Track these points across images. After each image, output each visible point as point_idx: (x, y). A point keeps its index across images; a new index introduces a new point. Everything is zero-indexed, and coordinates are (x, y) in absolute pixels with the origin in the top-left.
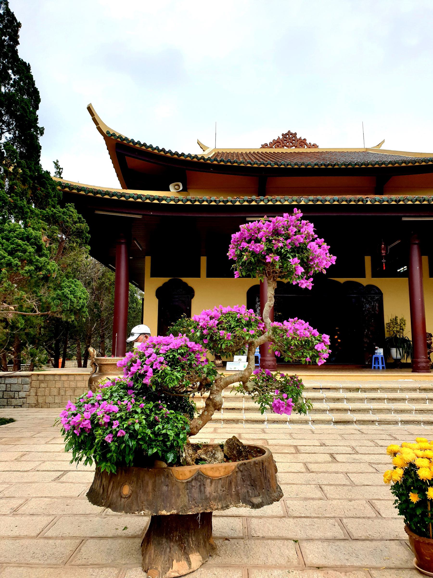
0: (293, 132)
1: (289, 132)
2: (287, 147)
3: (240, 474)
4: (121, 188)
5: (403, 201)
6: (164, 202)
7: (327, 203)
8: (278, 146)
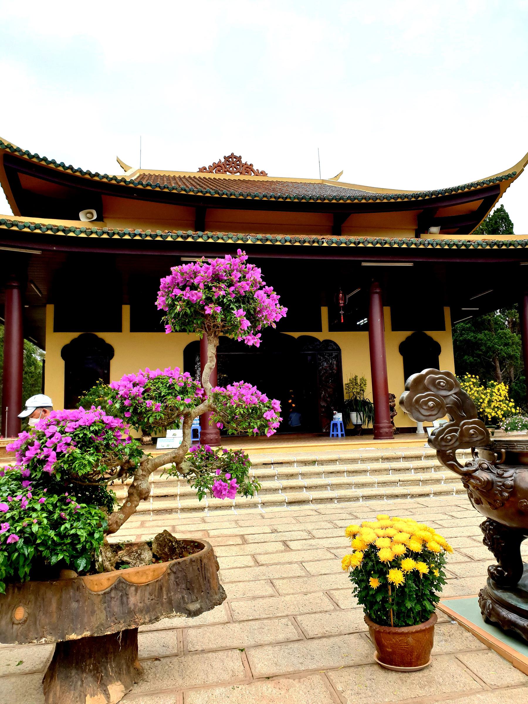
0: (237, 154)
1: (232, 154)
2: (231, 173)
3: (172, 577)
4: (13, 215)
5: (363, 243)
6: (71, 234)
7: (278, 243)
8: (219, 171)
